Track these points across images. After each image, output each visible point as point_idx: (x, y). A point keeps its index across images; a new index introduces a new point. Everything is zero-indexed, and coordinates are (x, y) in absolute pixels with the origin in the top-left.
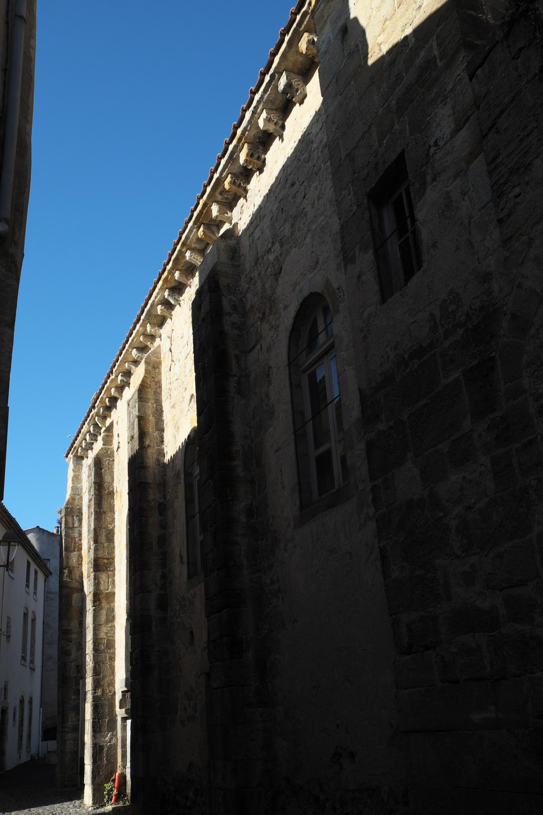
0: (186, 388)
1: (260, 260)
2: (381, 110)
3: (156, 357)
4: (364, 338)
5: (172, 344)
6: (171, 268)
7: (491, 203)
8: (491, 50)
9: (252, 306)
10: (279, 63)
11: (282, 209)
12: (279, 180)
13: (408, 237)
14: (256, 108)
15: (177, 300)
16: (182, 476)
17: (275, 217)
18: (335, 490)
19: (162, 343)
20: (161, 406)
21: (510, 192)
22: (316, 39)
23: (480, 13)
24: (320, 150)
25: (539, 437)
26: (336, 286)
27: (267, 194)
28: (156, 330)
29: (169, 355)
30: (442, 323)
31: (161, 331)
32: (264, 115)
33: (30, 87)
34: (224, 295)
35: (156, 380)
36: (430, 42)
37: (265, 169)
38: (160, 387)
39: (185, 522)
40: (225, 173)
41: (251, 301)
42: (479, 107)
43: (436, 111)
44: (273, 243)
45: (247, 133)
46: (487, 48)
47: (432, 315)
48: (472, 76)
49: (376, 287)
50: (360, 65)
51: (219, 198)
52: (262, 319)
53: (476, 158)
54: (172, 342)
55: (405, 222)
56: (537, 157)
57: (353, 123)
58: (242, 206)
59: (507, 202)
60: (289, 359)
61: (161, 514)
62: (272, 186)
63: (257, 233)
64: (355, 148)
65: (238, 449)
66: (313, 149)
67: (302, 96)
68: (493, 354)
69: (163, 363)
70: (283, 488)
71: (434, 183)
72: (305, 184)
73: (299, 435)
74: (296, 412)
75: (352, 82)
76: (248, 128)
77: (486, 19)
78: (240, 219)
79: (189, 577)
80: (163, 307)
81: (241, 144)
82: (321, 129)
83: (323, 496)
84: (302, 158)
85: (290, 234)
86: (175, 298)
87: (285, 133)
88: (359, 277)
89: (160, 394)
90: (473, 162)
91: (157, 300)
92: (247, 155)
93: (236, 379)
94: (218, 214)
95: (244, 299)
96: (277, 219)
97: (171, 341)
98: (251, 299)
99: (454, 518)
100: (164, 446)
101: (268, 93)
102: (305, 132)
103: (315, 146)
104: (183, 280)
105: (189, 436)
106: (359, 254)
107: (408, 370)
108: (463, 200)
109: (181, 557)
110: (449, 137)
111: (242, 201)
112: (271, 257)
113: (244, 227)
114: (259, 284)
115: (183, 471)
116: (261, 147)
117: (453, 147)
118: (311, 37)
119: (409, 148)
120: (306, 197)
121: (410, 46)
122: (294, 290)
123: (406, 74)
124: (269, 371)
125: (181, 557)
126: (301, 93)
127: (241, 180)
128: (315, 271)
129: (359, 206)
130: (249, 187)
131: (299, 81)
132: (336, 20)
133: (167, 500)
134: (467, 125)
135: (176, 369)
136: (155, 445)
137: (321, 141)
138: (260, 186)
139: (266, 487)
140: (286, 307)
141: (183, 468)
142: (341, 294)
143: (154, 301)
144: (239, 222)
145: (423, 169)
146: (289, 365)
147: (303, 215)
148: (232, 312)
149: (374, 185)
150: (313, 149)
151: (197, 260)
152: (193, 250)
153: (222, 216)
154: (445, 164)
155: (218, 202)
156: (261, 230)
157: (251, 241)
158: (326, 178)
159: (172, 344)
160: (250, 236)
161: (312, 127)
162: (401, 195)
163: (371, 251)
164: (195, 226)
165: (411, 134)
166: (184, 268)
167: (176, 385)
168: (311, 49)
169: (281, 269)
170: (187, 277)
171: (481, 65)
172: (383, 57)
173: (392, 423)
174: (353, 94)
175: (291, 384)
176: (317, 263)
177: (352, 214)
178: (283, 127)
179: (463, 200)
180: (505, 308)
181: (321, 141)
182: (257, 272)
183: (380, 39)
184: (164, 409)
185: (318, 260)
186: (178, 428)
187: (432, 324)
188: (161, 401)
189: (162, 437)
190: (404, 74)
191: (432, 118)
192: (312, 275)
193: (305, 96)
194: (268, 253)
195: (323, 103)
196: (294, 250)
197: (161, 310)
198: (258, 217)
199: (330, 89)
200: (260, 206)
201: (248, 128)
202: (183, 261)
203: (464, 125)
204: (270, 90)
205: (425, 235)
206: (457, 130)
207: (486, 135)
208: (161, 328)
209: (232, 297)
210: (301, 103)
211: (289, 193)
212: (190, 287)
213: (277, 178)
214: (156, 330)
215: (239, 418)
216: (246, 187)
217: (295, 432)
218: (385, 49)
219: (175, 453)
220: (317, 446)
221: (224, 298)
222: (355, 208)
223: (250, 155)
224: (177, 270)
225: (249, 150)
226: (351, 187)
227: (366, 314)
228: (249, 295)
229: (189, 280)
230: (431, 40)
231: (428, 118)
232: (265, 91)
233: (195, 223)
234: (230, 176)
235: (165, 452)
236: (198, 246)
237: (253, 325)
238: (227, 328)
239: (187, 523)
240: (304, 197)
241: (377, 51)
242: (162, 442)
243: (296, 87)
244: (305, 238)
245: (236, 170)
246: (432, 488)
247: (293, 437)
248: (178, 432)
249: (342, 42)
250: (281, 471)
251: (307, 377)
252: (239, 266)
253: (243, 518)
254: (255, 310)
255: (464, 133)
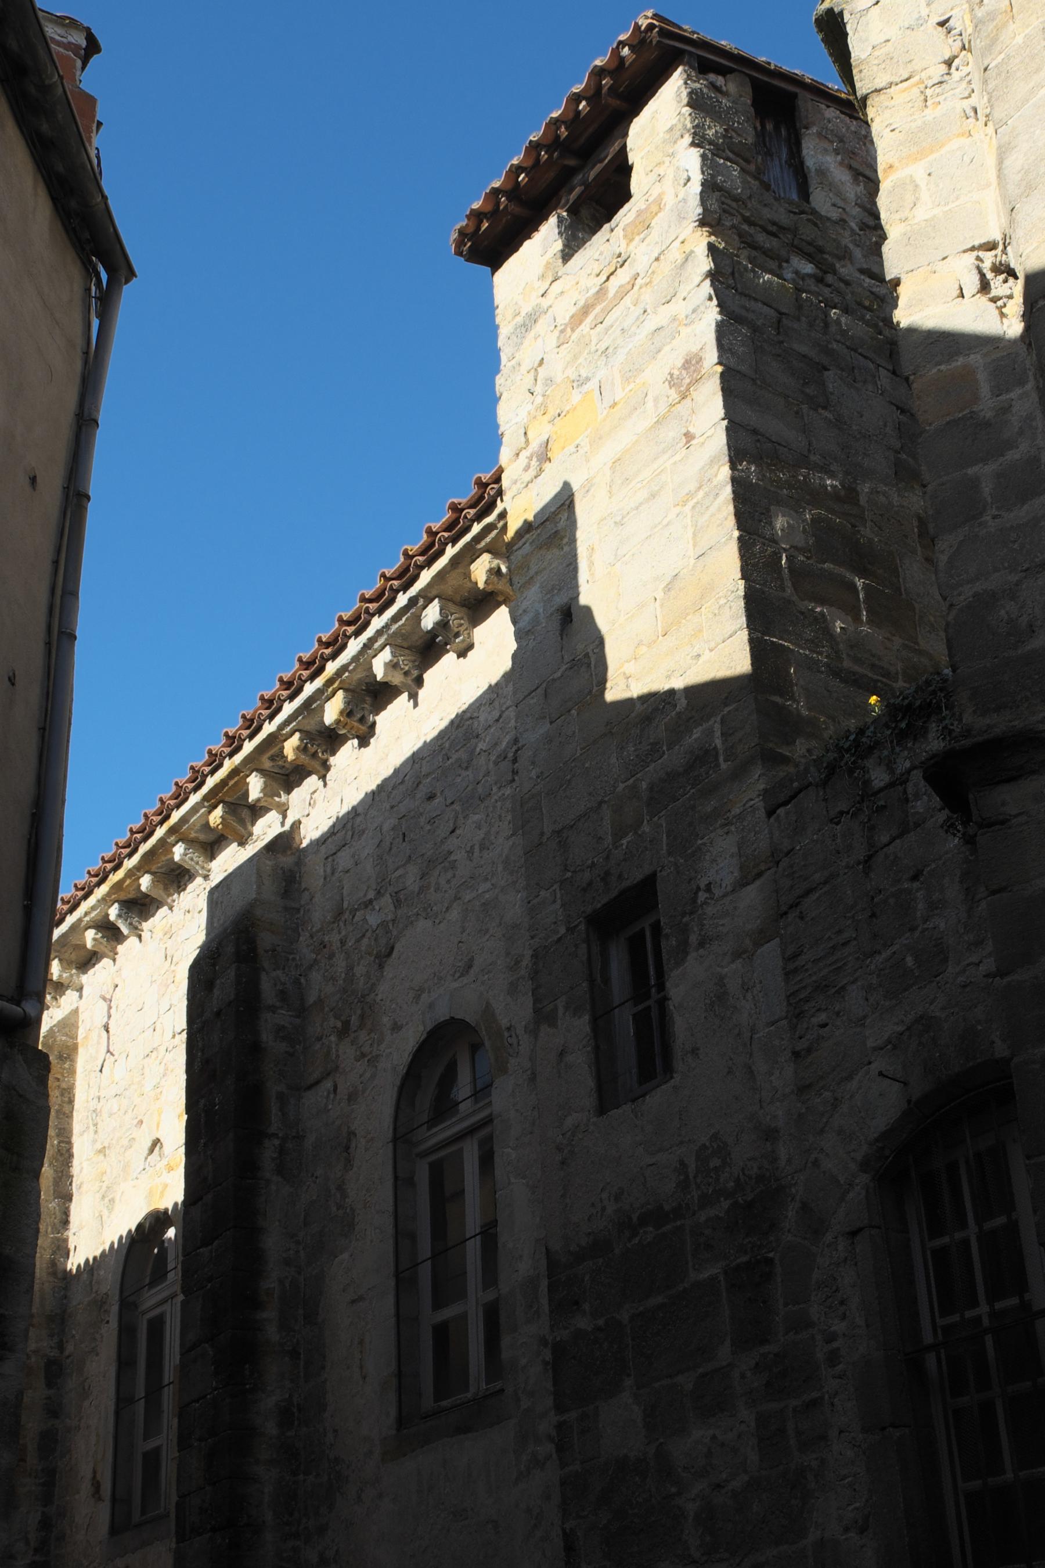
0: (141, 1122)
1: (347, 915)
2: (622, 786)
3: (67, 1035)
4: (563, 1163)
5: (109, 1017)
6: (134, 867)
7: (785, 1022)
8: (800, 791)
9: (320, 1001)
10: (429, 585)
11: (404, 834)
12: (401, 776)
13: (649, 1007)
14: (372, 640)
15: (136, 928)
16: (115, 1309)
17: (388, 843)
18: (469, 1395)
19: (83, 1004)
20: (69, 1143)
21: (813, 1016)
22: (504, 569)
23: (789, 700)
24: (493, 758)
25: (827, 1397)
26: (504, 1022)
27: (373, 792)
28: (72, 976)
29: (99, 1036)
30: (698, 1181)
31: (84, 979)
32: (386, 655)
33: (220, 944)
34: (264, 970)
35: (64, 1085)
36: (710, 723)
37: (372, 740)
38: (71, 1101)
39: (112, 1408)
40: (288, 729)
41: (320, 991)
42: (778, 863)
43: (712, 835)
44: (379, 894)
45: (347, 674)
46: (795, 784)
47: (682, 1163)
48: (770, 813)
49: (591, 1083)
50: (591, 691)
51: (267, 764)
52: (344, 1031)
53: (769, 941)
54: (113, 1011)
55: (648, 979)
56: (853, 982)
57: (569, 781)
58: (315, 792)
59: (807, 1028)
60: (395, 1129)
61: (49, 1384)
62: (386, 781)
63: (344, 859)
64: (572, 827)
65: (272, 1286)
66: (478, 750)
67: (463, 646)
68: (771, 1255)
69: (81, 1050)
70: (364, 1378)
71: (701, 951)
72: (457, 807)
73: (404, 1280)
74: (403, 1235)
75: (573, 712)
76: (351, 668)
77: (797, 708)
78: (308, 815)
79: (114, 1530)
80: (100, 935)
81: (330, 689)
82: (497, 720)
83: (445, 1403)
84: (455, 757)
85: (417, 890)
86: (131, 924)
87: (422, 693)
88: (562, 1054)
89: (70, 1116)
90: (762, 945)
91: (87, 919)
92: (341, 713)
93: (277, 1142)
94: (261, 795)
95: (303, 980)
96: (390, 849)
97: (110, 1008)
98: (317, 985)
99: (693, 1499)
100: (70, 1234)
101: (400, 623)
102: (464, 712)
103: (482, 746)
104: (158, 893)
105: (140, 1226)
106: (564, 1014)
107: (636, 1240)
108: (744, 997)
109: (97, 1486)
110: (729, 888)
111: (312, 782)
112: (373, 920)
113: (316, 835)
114: (340, 964)
115: (117, 1298)
116: (368, 699)
117: (735, 908)
118: (496, 562)
119: (664, 873)
120: (458, 832)
121: (678, 709)
122: (417, 998)
123: (668, 750)
124: (349, 1140)
125: (97, 1486)
126: (463, 641)
127: (318, 746)
128: (465, 980)
129: (570, 930)
130: (333, 760)
131: (462, 618)
132: (552, 589)
133: (67, 1353)
134: (758, 883)
135: (118, 1072)
136: (50, 1229)
137: (496, 744)
138: (356, 774)
139: (323, 1368)
140: (396, 1027)
141: (117, 1292)
142: (514, 1041)
143: (80, 920)
144: (303, 820)
145: (685, 920)
146: (395, 1140)
147: (446, 864)
148: (278, 1004)
149: (599, 905)
150: (478, 750)
151: (197, 863)
152: (190, 842)
153: (269, 799)
154: (721, 928)
155: (262, 772)
156: (353, 856)
157: (329, 870)
158: (500, 816)
159: (109, 1017)
160: (327, 858)
161: (479, 708)
162: (643, 930)
163: (587, 1017)
164: (206, 804)
165: (670, 854)
166: (163, 870)
167: (115, 1109)
168: (493, 583)
169: (392, 948)
170: (166, 889)
171: (785, 804)
172: (630, 701)
173: (601, 1322)
174: (574, 733)
175: (396, 1178)
176: (470, 967)
177: (556, 937)
178: (419, 682)
179: (744, 997)
180: (793, 1190)
181: (496, 744)
182: (337, 937)
183: (630, 668)
184: (76, 1150)
185: (472, 959)
186: (112, 1201)
187: (682, 1177)
188: (71, 1132)
189: (66, 1213)
190: (665, 748)
191: (704, 844)
192: (456, 985)
193: (471, 647)
194: (366, 907)
195: (507, 677)
196: (422, 924)
197: (94, 939)
198: (347, 828)
199: (532, 702)
200: (354, 808)
201: (351, 668)
202: (164, 858)
203: (754, 880)
204: (404, 619)
205: (680, 1026)
206: (743, 883)
207: (786, 913)
208: (85, 972)
209: (279, 973)
210: (462, 654)
211: (421, 810)
212: (171, 908)
213: (396, 771)
214: (72, 976)
215: (277, 1223)
216: (327, 760)
217: (397, 1274)
218: (636, 690)
219: (98, 1253)
220: (437, 1305)
221: (264, 977)
222: (562, 930)
223: (348, 713)
224: (147, 872)
225: (347, 703)
226: (558, 891)
227: (569, 1122)
228: (316, 976)
229: (170, 895)
230: (713, 720)
231: (700, 842)
232: (395, 619)
233: (205, 798)
234: (297, 735)
235: (71, 1246)
236: (202, 837)
237: (319, 1039)
238: (266, 1037)
239: (117, 1413)
240: (453, 831)
241: (623, 686)
242: (66, 1222)
243: (456, 630)
244: (448, 909)
245: (311, 725)
246: (661, 1444)
247: (392, 1283)
248: (110, 1210)
249: (561, 635)
250: (361, 1342)
251: (427, 1166)
252: (298, 910)
253: (271, 1428)
254: (327, 1009)
255: (752, 894)
